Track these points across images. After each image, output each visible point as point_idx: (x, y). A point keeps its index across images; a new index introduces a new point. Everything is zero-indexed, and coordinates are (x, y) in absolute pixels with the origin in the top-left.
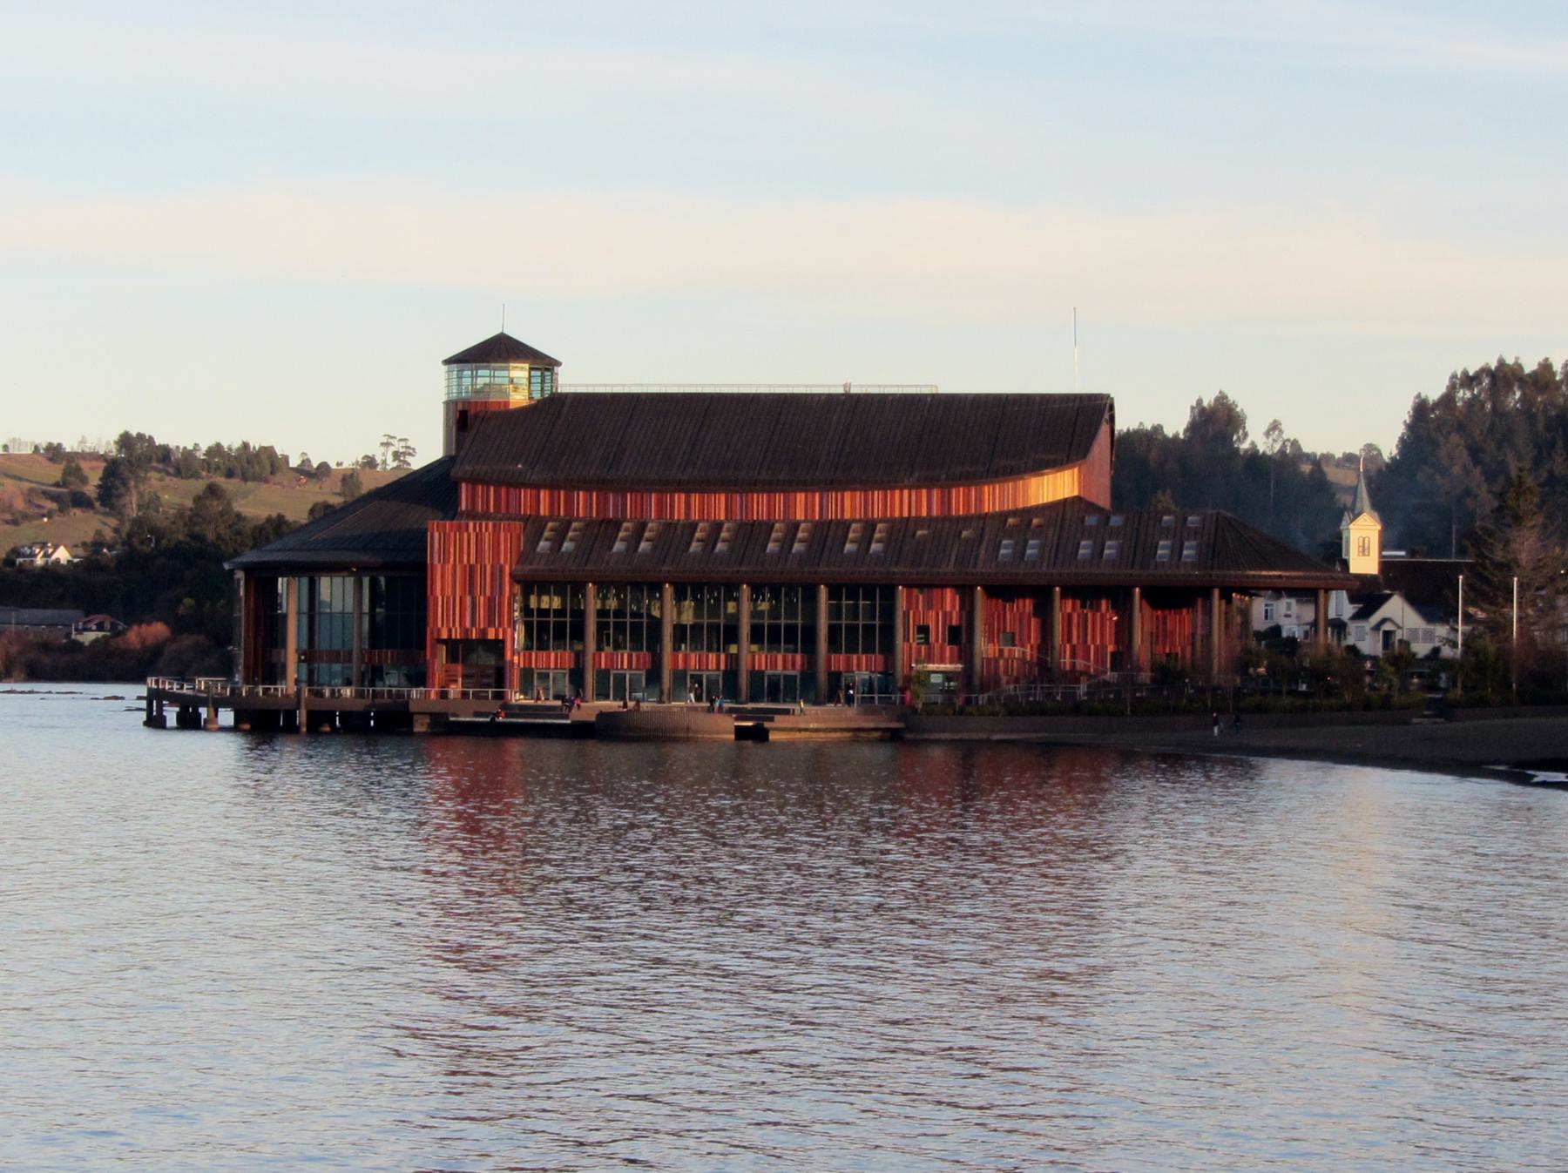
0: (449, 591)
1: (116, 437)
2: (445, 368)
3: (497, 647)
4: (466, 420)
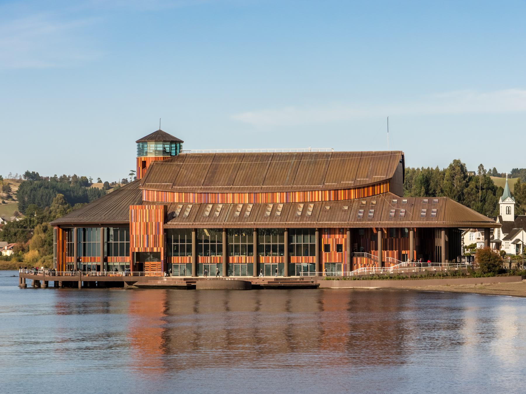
0: (138, 233)
1: (24, 173)
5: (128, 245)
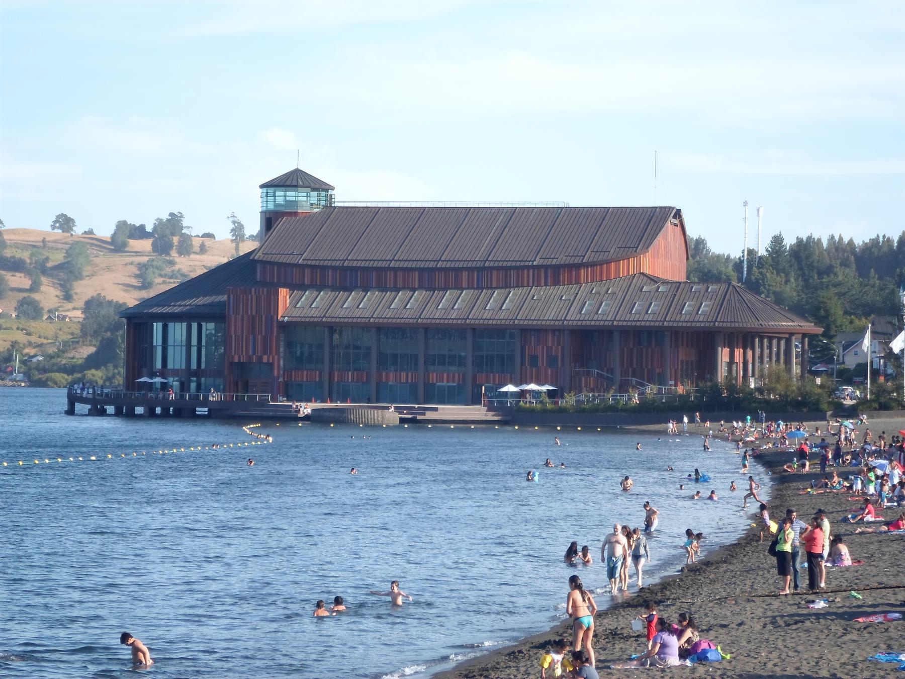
0: (239, 333)
2: (260, 190)
4: (270, 220)
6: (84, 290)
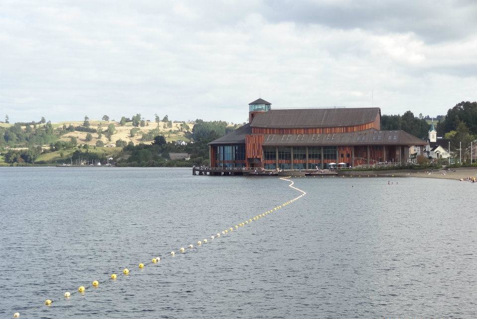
3: (259, 159)
4: (252, 115)
5: (245, 155)
6: (115, 138)
